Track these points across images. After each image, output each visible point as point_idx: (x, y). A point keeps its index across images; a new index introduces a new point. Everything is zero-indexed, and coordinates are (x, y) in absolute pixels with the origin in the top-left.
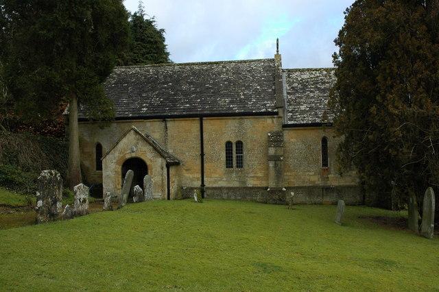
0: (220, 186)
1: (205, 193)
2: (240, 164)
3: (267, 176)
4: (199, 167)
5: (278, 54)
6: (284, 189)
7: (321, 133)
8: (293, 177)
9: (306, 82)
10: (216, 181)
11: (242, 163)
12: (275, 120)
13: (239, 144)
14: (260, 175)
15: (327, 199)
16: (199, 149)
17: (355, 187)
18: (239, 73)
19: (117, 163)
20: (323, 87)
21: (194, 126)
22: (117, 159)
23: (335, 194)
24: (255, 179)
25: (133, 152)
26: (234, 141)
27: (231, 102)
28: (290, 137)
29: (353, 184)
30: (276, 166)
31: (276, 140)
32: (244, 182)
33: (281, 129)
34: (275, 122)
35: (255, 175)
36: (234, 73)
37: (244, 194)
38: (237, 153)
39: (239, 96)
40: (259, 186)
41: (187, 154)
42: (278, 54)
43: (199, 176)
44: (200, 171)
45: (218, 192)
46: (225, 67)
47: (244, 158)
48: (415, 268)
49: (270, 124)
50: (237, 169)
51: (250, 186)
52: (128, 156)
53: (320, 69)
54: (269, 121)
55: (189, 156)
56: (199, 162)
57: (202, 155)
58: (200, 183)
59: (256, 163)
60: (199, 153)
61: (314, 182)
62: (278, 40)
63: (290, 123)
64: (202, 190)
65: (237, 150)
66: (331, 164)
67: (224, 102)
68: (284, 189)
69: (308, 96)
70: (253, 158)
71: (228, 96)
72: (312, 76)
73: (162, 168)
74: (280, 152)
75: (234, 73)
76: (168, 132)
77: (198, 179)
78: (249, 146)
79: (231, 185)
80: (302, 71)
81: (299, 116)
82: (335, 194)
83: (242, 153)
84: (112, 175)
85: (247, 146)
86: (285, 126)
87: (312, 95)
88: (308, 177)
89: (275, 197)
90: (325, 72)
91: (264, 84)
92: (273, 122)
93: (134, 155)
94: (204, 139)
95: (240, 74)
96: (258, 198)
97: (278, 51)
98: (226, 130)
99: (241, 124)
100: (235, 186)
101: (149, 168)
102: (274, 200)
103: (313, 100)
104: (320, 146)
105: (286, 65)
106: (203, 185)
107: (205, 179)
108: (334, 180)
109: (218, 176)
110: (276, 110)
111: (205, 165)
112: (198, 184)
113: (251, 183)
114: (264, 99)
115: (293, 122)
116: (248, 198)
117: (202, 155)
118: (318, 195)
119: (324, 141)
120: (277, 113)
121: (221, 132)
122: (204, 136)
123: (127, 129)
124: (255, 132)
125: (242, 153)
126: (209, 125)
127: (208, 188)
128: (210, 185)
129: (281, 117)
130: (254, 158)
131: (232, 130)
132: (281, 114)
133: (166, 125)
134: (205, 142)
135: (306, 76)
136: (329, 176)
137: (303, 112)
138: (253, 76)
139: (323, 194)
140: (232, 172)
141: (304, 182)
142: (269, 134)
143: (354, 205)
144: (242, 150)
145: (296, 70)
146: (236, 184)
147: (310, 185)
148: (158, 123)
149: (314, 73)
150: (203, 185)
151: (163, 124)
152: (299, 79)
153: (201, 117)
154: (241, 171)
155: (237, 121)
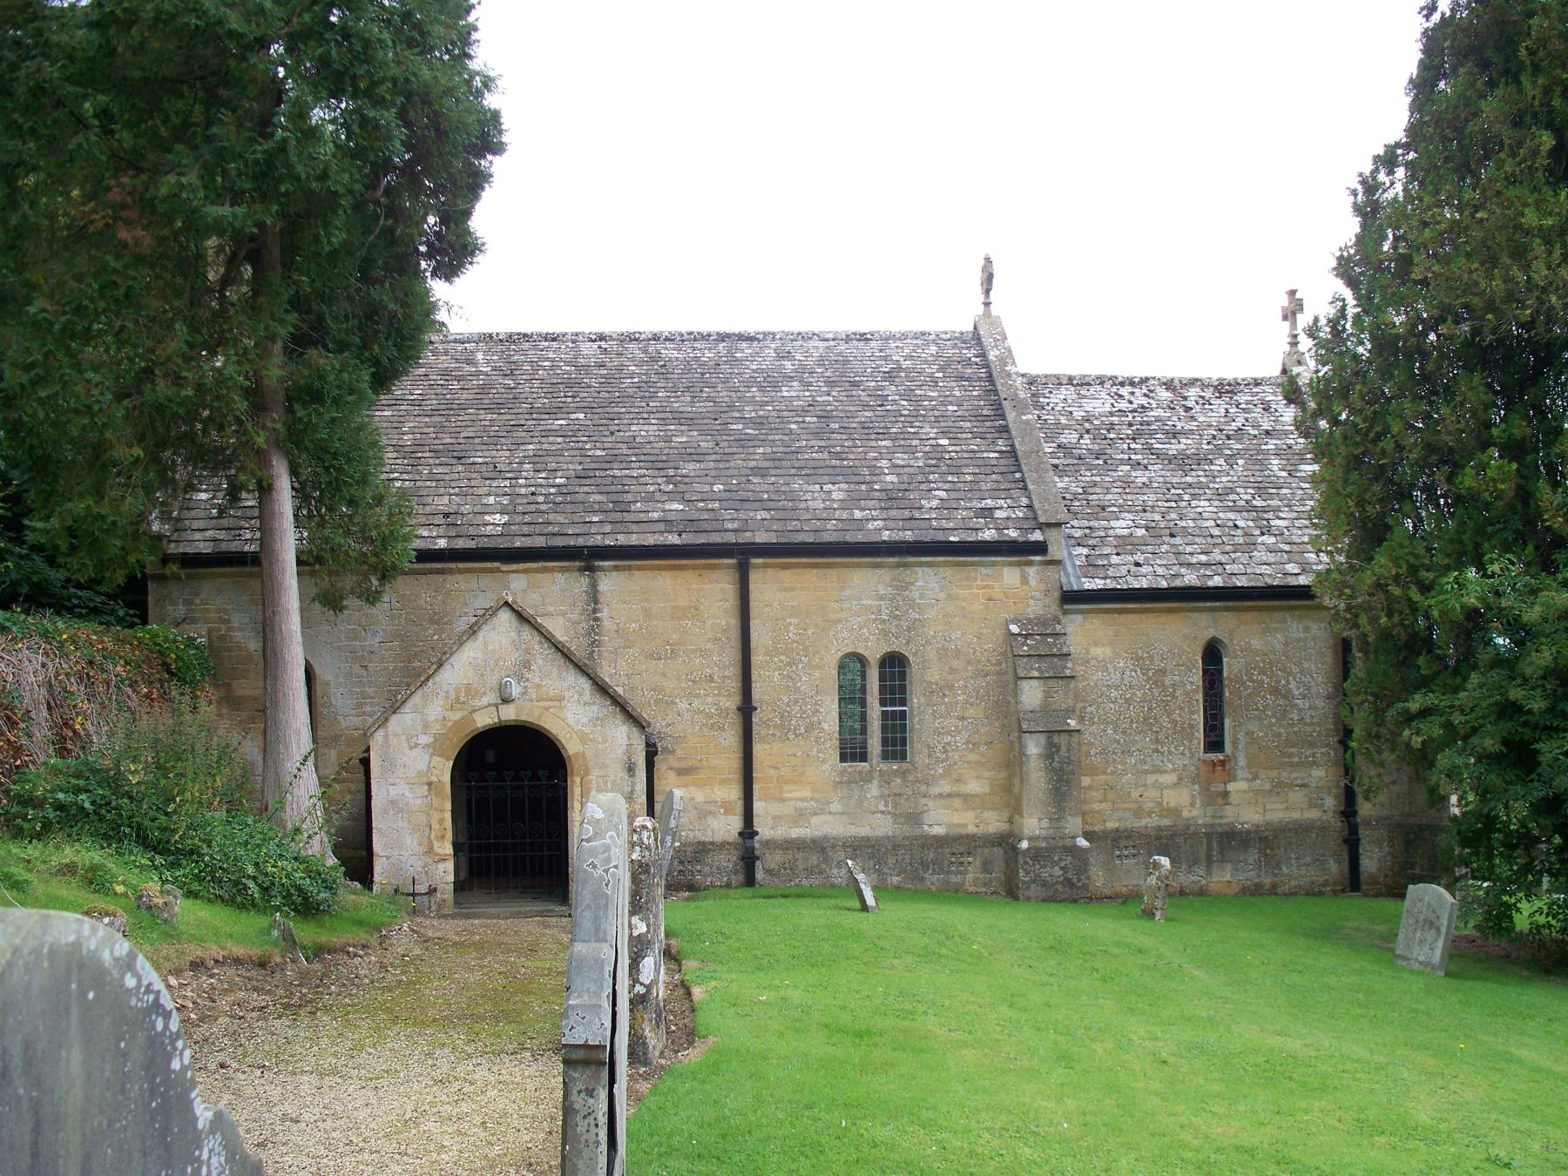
0: (817, 833)
1: (758, 863)
2: (896, 744)
3: (1010, 798)
4: (733, 760)
5: (987, 314)
6: (1082, 842)
7: (1201, 625)
8: (1098, 795)
9: (1152, 423)
10: (800, 816)
11: (904, 742)
12: (1032, 571)
13: (894, 666)
14: (975, 786)
15: (1224, 877)
16: (734, 685)
17: (1322, 829)
18: (854, 388)
19: (436, 748)
20: (1173, 448)
21: (711, 591)
22: (437, 728)
23: (1252, 856)
24: (958, 803)
25: (506, 701)
26: (874, 652)
27: (851, 502)
28: (1088, 637)
29: (1314, 814)
30: (1051, 751)
31: (1037, 649)
32: (914, 818)
33: (1054, 609)
34: (1033, 582)
35: (955, 793)
36: (831, 383)
37: (920, 866)
38: (883, 703)
39: (876, 472)
40: (971, 829)
41: (683, 705)
42: (987, 314)
43: (734, 793)
44: (736, 777)
45: (814, 859)
46: (788, 356)
47: (914, 722)
48: (197, 965)
49: (1016, 589)
50: (884, 766)
51: (939, 830)
52: (484, 720)
53: (1144, 381)
54: (1008, 576)
55: (696, 717)
56: (730, 739)
57: (746, 710)
58: (735, 823)
59: (960, 740)
60: (732, 702)
61: (1176, 812)
62: (988, 261)
63: (1090, 584)
64: (748, 855)
65: (882, 689)
66: (1235, 742)
67: (824, 505)
68: (1082, 842)
69: (1127, 483)
70: (947, 721)
71: (836, 474)
72: (1123, 405)
73: (631, 770)
74: (1061, 700)
75: (831, 383)
76: (604, 614)
77: (727, 808)
78: (934, 675)
79: (864, 831)
80: (1081, 383)
81: (1115, 559)
82: (1252, 856)
83: (903, 702)
84: (415, 797)
85: (924, 676)
86: (1072, 598)
87: (1140, 477)
88: (1153, 794)
89: (1011, 872)
90: (1164, 395)
91: (962, 430)
92: (1025, 580)
93: (509, 714)
94: (753, 644)
95: (855, 384)
96: (972, 875)
97: (987, 304)
98: (842, 614)
99: (902, 587)
100: (880, 832)
101: (574, 766)
102: (1045, 884)
103: (1150, 498)
104: (1197, 677)
105: (1032, 353)
106: (748, 831)
107: (758, 806)
108: (1248, 805)
109: (810, 796)
110: (1037, 536)
111: (758, 749)
112: (727, 827)
113: (940, 820)
114: (974, 489)
115: (1098, 584)
116: (933, 879)
117: (746, 710)
118: (1213, 867)
119: (1212, 654)
120: (1041, 548)
121: (821, 622)
122: (754, 635)
123: (485, 601)
124: (959, 618)
125: (903, 702)
126: (774, 589)
127: (768, 844)
128: (780, 833)
129: (1058, 562)
130: (951, 723)
131: (867, 608)
132: (1056, 551)
133: (594, 585)
134: (757, 658)
135: (1099, 404)
136: (1231, 787)
137: (1126, 544)
138: (916, 401)
139: (1209, 857)
140: (866, 778)
141: (1139, 812)
142: (1014, 629)
143: (1320, 894)
144: (903, 689)
145: (1059, 381)
146: (880, 826)
147: (1166, 822)
148: (560, 578)
149: (1125, 391)
150: (748, 831)
151: (584, 581)
152: (1078, 414)
153: (742, 557)
154: (903, 774)
155: (885, 574)
